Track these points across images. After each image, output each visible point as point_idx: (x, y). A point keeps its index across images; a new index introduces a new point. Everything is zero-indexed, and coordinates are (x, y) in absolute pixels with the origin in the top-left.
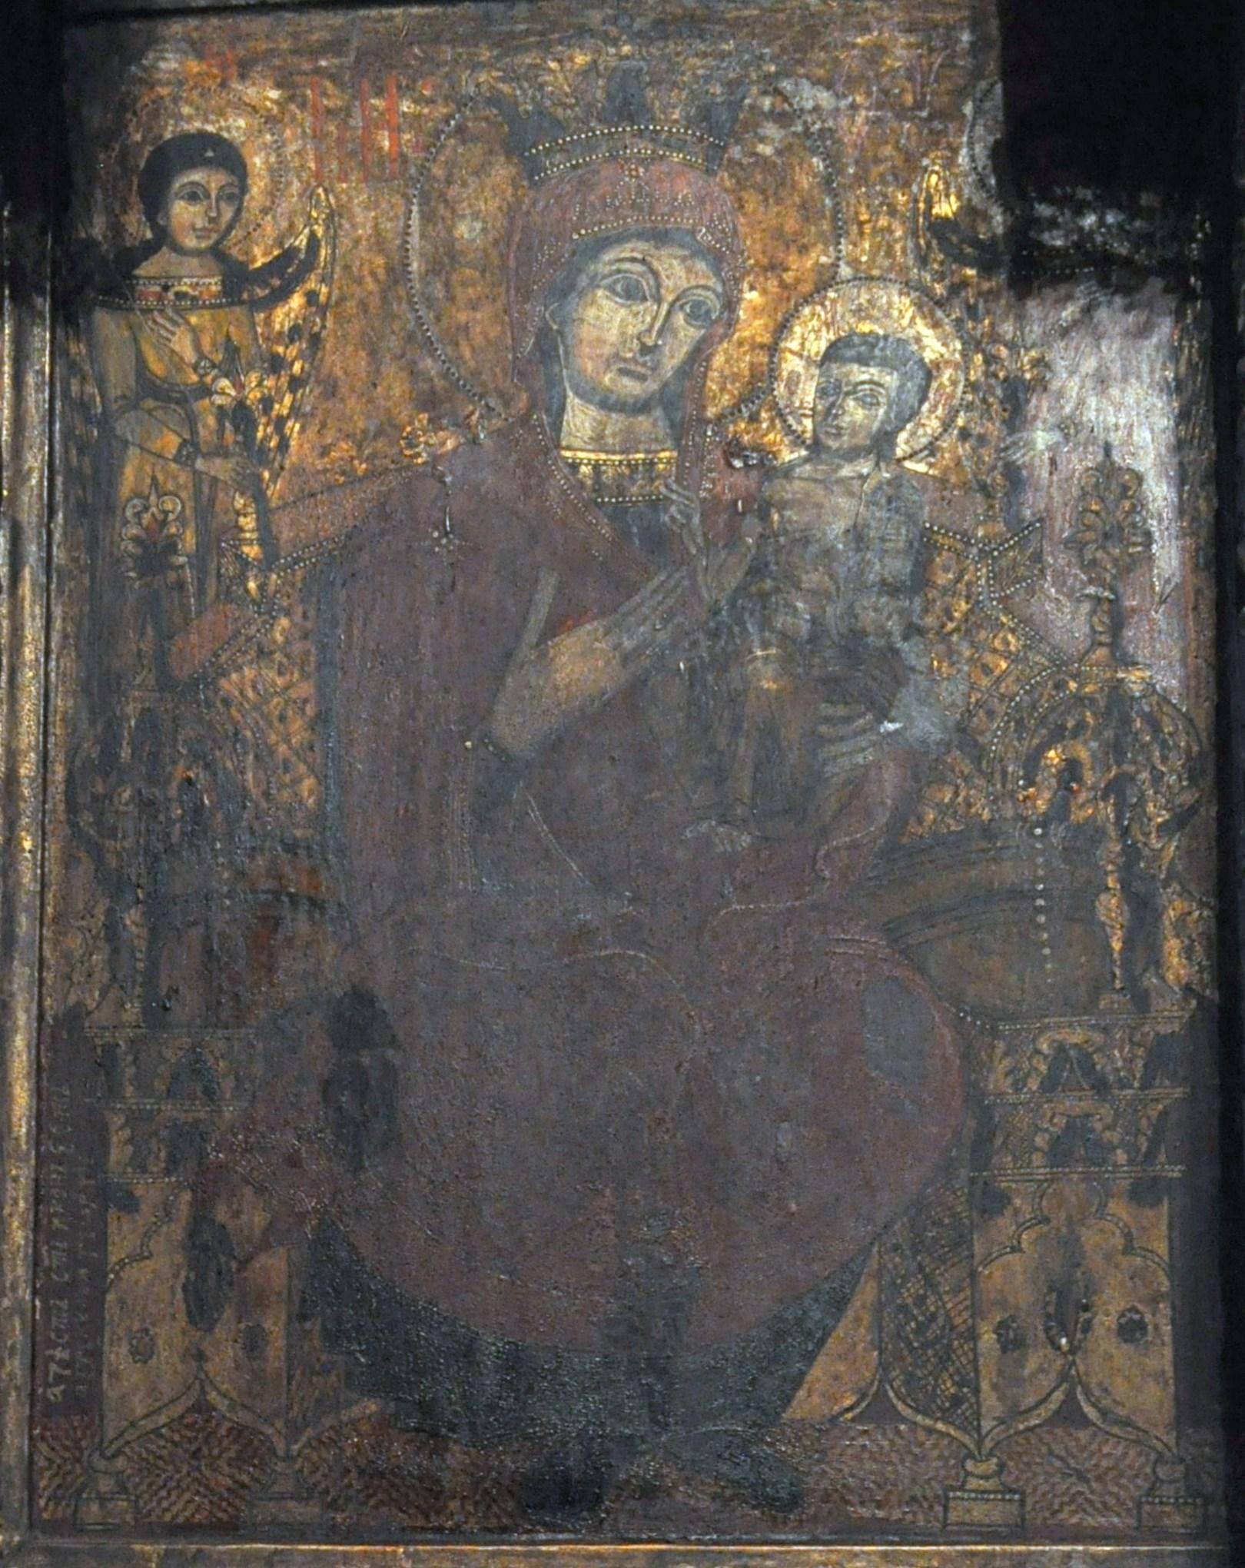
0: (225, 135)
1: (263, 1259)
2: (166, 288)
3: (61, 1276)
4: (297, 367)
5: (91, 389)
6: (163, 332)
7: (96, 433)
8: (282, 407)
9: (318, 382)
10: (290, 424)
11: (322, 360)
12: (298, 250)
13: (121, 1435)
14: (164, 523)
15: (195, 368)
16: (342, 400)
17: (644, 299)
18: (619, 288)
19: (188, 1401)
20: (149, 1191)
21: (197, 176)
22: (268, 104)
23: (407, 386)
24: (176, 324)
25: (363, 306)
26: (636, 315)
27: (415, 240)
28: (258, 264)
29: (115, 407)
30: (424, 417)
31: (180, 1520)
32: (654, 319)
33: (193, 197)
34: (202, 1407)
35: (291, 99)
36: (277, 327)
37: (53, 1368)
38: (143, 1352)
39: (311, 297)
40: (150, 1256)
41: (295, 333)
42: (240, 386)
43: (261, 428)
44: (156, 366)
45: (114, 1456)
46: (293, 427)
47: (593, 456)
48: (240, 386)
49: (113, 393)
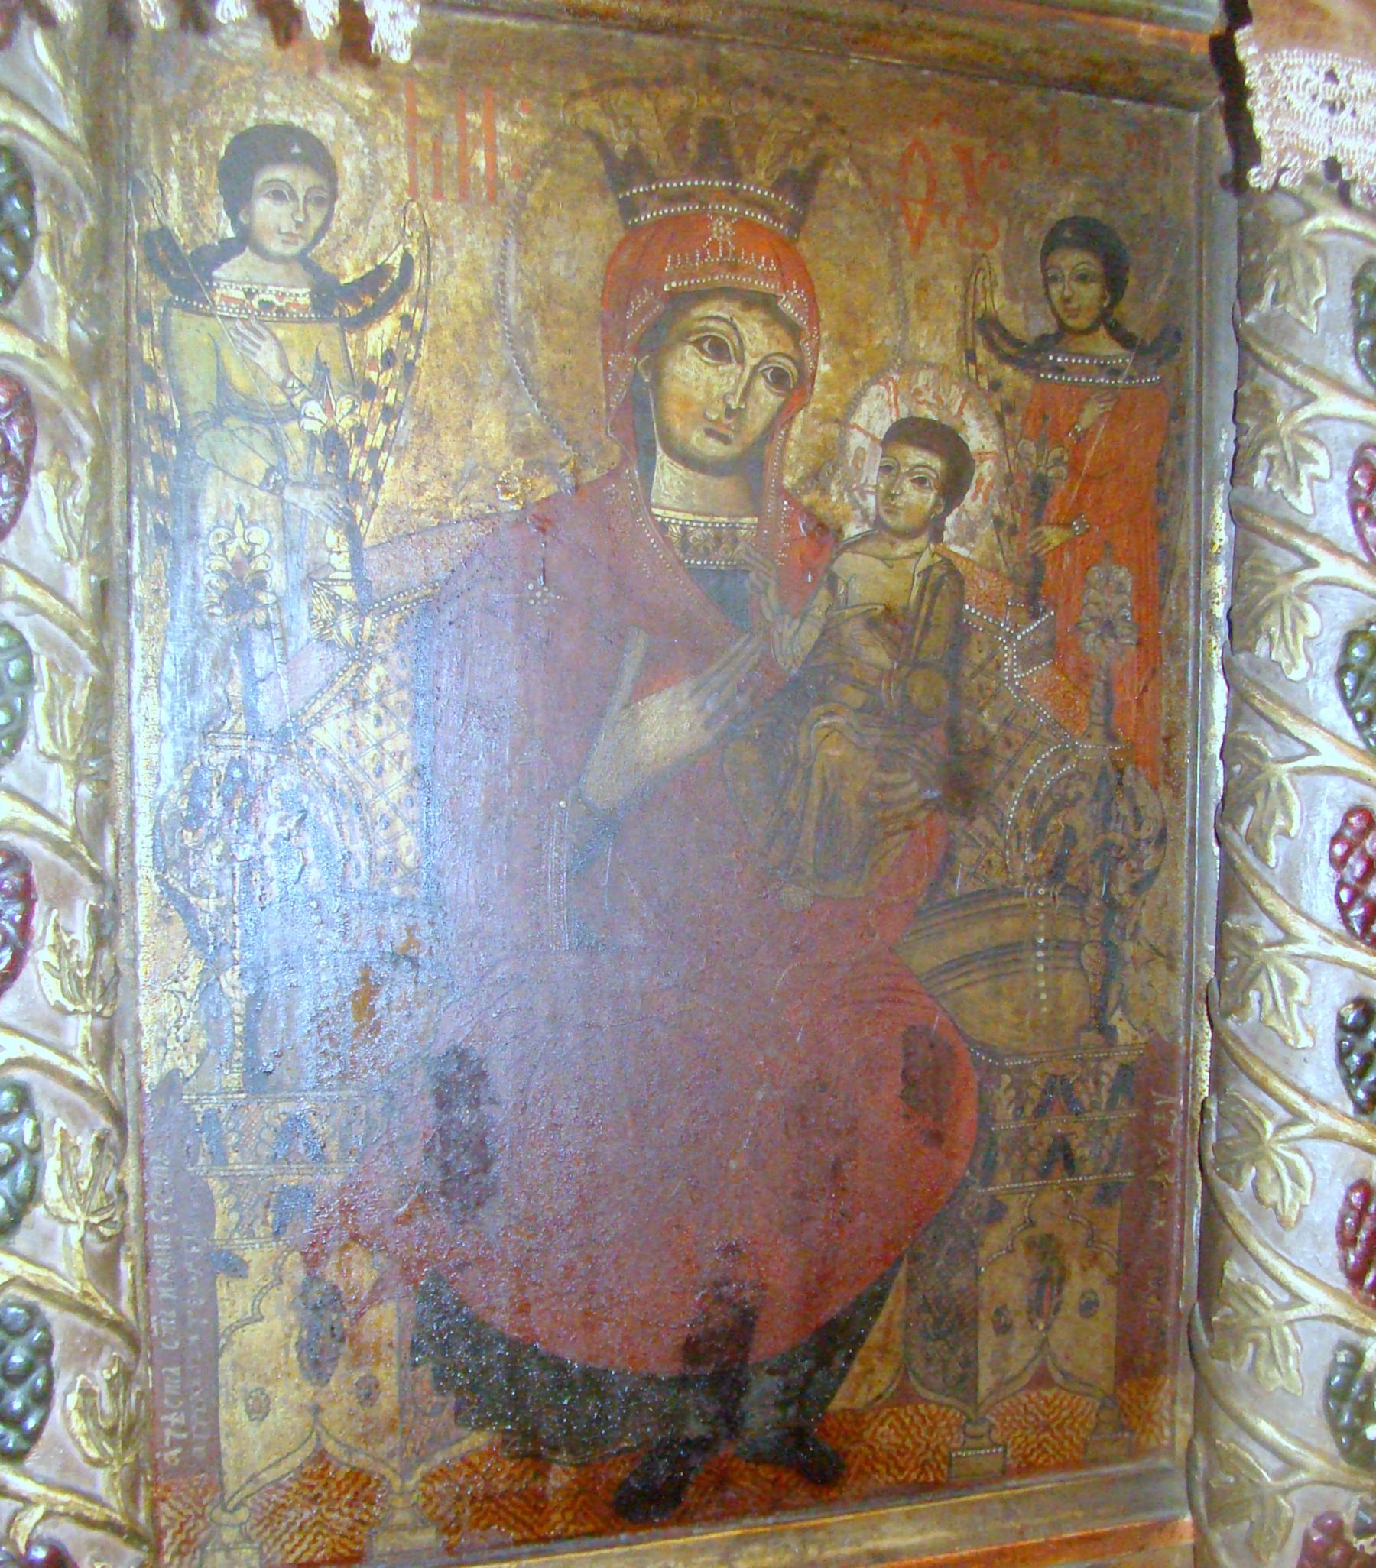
0: (314, 132)
1: (372, 1315)
2: (250, 294)
3: (171, 1343)
4: (390, 398)
5: (166, 400)
6: (246, 343)
7: (174, 451)
8: (375, 440)
9: (414, 415)
10: (384, 456)
11: (415, 391)
12: (391, 268)
13: (242, 1488)
14: (251, 557)
15: (283, 386)
16: (438, 436)
17: (729, 361)
18: (706, 345)
19: (308, 1451)
20: (256, 1255)
21: (282, 173)
22: (358, 102)
23: (503, 428)
24: (262, 338)
25: (458, 336)
26: (722, 375)
27: (512, 275)
28: (348, 280)
29: (196, 423)
30: (521, 461)
31: (304, 1559)
32: (738, 381)
33: (278, 196)
34: (321, 1455)
35: (385, 101)
36: (370, 351)
37: (168, 1433)
38: (259, 1409)
39: (406, 321)
40: (262, 1319)
41: (388, 359)
42: (329, 410)
43: (354, 459)
44: (239, 379)
45: (236, 1508)
46: (387, 461)
47: (680, 515)
48: (329, 410)
49: (192, 408)
